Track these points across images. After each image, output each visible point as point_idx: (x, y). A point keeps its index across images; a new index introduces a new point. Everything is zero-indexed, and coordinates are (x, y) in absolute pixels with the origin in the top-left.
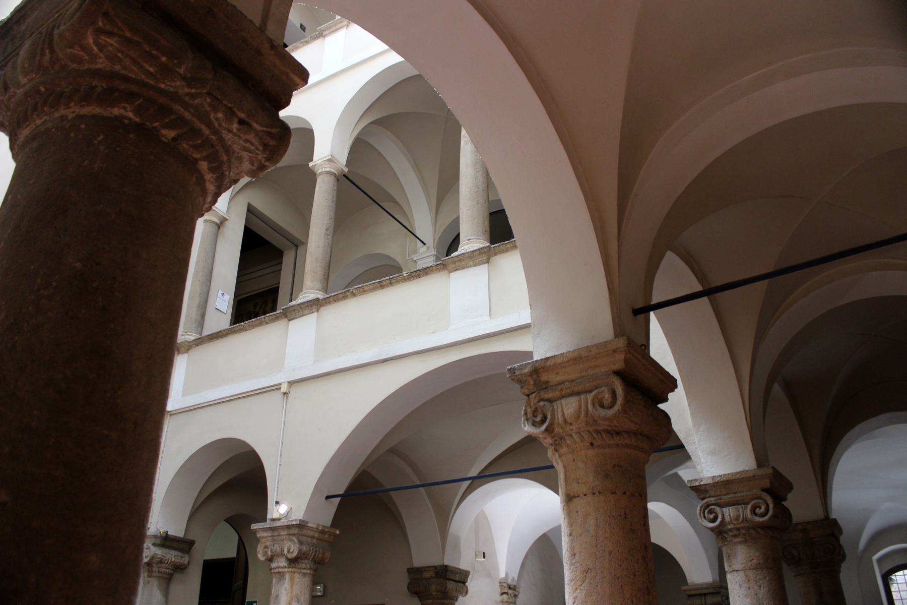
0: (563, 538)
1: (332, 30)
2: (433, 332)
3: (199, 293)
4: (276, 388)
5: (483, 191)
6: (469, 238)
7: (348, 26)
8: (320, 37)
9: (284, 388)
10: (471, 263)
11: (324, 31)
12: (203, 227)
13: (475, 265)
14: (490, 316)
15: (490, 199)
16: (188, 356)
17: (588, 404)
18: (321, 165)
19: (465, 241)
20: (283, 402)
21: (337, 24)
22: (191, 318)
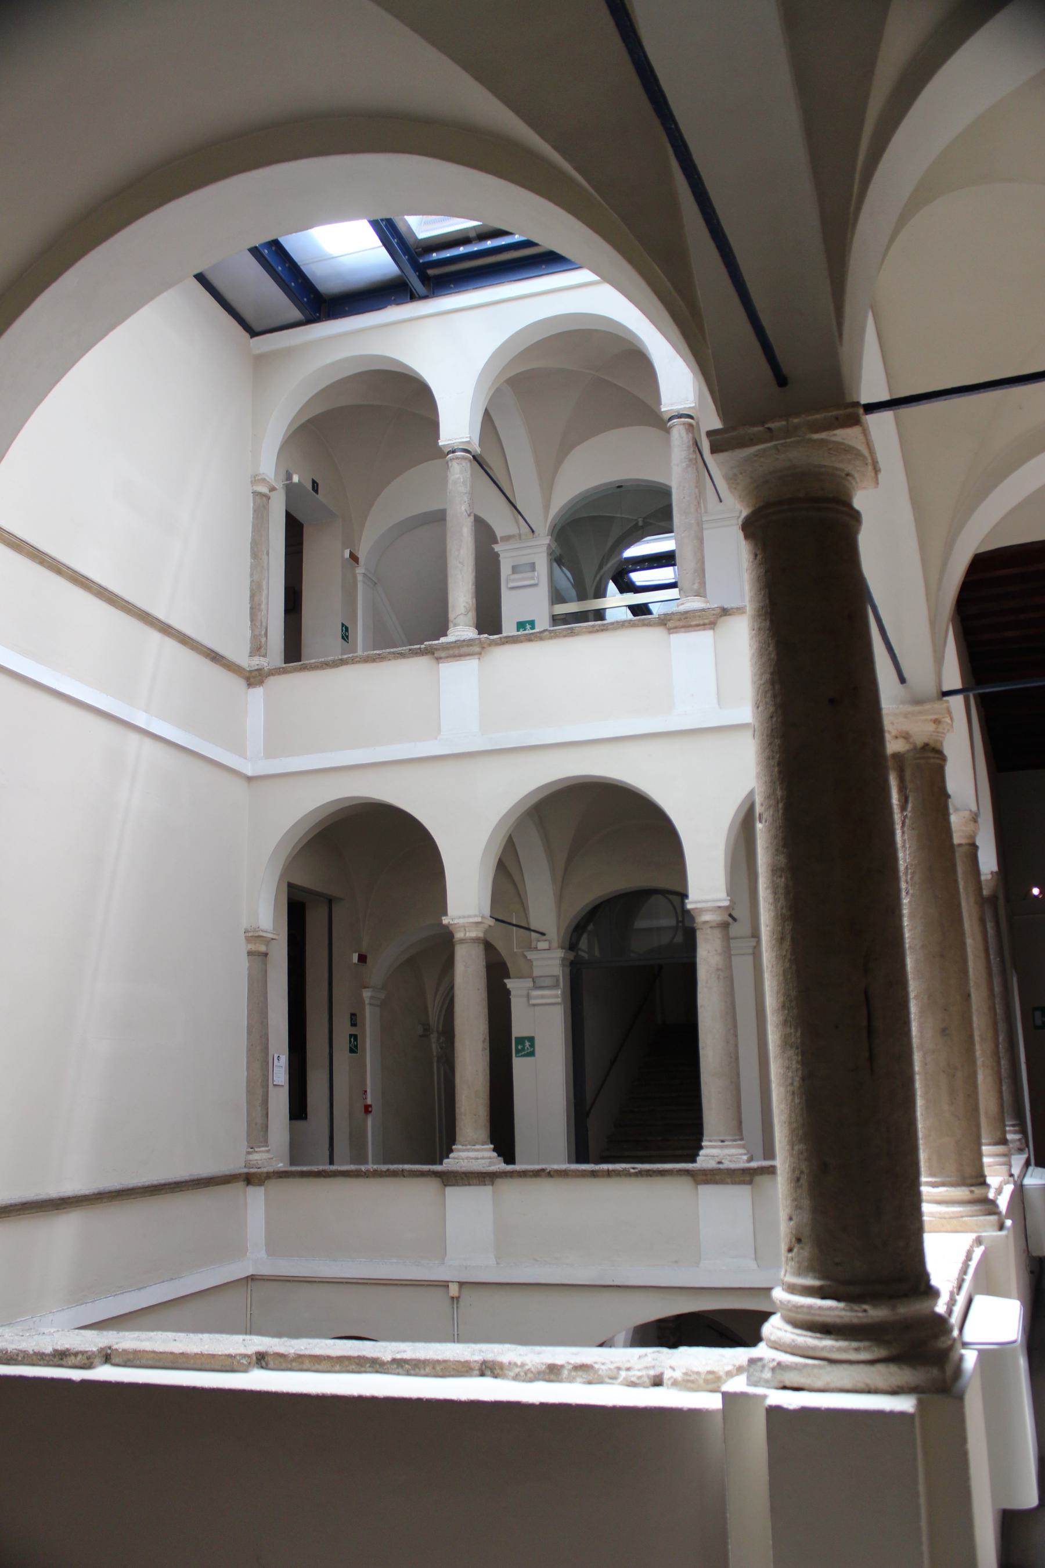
0: (901, 855)
1: (451, 652)
2: (676, 1262)
3: (260, 1081)
4: (445, 1285)
5: (718, 970)
6: (722, 1138)
7: (480, 654)
8: (426, 653)
9: (454, 1290)
10: (729, 1180)
11: (437, 649)
12: (247, 965)
13: (732, 1184)
14: (756, 1259)
15: (650, 605)
16: (265, 1190)
17: (969, 1006)
18: (464, 927)
19: (715, 1141)
20: (453, 1308)
21: (462, 646)
22: (256, 1124)
